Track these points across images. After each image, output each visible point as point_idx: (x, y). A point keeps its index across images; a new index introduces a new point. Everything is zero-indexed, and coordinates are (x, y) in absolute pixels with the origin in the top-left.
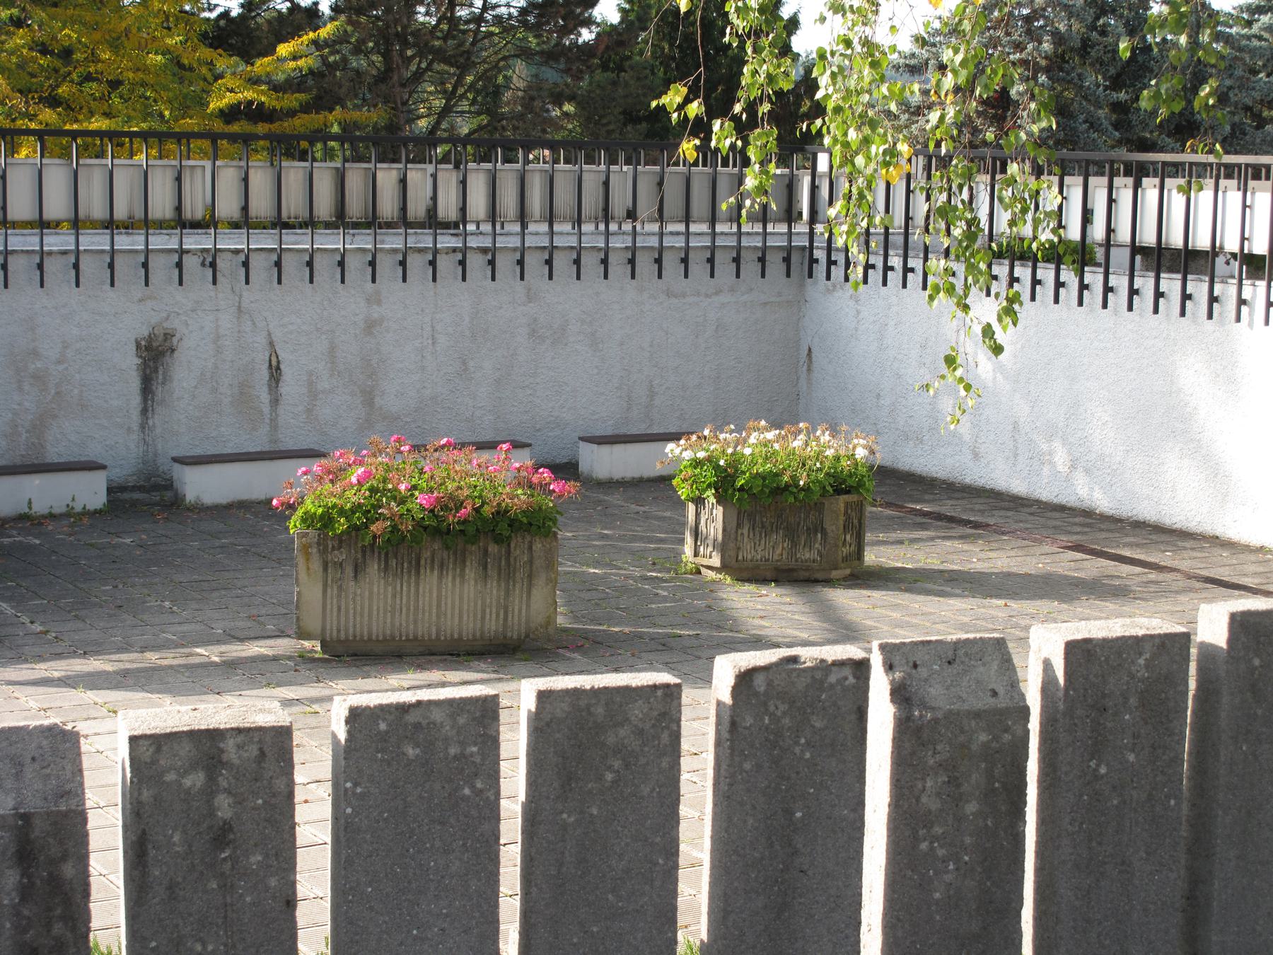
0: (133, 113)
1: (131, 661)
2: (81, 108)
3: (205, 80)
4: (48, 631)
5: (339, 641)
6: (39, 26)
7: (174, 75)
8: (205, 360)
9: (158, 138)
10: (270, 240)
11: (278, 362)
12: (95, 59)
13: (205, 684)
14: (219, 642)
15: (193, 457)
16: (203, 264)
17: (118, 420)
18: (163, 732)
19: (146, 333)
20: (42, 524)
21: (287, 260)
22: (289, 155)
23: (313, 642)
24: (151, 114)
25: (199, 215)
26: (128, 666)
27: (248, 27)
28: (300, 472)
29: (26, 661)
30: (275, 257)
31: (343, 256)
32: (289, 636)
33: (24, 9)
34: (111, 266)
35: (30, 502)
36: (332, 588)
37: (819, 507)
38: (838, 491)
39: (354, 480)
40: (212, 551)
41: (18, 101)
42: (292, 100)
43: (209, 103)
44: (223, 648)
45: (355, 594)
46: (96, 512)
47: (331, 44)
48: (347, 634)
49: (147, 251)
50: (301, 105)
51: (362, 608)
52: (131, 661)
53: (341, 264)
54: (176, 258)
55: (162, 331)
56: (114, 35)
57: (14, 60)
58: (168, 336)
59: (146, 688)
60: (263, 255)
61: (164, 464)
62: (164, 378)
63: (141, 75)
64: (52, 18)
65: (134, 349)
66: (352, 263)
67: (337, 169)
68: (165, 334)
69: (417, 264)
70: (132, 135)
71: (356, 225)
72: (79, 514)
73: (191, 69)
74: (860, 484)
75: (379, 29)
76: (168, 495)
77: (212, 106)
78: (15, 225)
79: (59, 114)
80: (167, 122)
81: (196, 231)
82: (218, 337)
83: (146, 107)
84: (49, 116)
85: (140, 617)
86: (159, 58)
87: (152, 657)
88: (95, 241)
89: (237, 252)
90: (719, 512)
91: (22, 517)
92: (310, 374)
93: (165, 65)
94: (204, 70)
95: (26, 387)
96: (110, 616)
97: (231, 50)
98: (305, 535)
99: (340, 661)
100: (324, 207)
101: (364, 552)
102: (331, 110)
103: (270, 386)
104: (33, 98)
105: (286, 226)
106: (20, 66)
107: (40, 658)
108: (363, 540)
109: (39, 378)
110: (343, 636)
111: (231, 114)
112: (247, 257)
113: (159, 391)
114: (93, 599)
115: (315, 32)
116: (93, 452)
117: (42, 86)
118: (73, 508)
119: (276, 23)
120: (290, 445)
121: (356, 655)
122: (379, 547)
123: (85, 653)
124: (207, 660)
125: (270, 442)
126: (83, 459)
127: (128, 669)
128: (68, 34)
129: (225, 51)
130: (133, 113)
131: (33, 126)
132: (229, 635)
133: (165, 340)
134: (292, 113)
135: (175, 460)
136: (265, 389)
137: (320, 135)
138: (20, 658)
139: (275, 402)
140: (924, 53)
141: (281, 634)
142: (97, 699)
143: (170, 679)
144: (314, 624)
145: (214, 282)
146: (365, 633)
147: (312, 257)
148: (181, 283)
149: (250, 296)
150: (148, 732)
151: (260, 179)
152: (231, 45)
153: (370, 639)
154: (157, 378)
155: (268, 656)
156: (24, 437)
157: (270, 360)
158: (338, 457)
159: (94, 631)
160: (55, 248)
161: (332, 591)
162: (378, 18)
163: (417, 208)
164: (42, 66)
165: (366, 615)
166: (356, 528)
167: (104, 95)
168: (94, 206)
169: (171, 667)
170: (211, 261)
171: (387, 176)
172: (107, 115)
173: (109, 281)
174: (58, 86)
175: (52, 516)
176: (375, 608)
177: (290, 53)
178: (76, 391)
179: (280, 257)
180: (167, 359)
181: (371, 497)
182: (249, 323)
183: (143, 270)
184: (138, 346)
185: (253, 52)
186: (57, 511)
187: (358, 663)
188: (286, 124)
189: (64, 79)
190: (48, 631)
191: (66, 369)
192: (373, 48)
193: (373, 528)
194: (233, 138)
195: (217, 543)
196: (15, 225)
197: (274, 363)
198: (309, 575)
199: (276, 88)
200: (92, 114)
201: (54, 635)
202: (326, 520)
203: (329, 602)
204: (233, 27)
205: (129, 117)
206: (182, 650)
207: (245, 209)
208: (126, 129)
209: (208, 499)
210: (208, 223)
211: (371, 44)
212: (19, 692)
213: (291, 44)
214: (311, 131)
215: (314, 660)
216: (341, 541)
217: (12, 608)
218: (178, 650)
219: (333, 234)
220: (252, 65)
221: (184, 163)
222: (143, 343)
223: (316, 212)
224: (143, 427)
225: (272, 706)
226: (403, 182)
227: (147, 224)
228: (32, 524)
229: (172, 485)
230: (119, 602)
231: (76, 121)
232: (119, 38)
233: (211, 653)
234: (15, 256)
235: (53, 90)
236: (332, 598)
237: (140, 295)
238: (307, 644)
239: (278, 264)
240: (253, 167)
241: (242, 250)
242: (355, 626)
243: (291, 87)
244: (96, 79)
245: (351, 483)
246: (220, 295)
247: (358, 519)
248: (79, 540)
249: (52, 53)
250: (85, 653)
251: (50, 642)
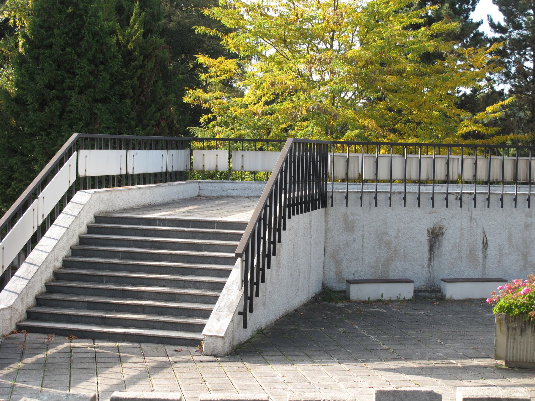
0: (426, 136)
1: (424, 364)
2: (405, 133)
3: (456, 122)
4: (390, 349)
5: (513, 361)
6: (390, 100)
7: (443, 120)
8: (456, 239)
9: (437, 146)
10: (484, 189)
11: (487, 241)
12: (411, 113)
13: (455, 375)
14: (461, 358)
15: (450, 279)
16: (456, 199)
17: (419, 262)
18: (477, 397)
19: (432, 227)
20: (387, 304)
21: (492, 198)
22: (494, 153)
23: (502, 361)
24: (433, 136)
25: (455, 178)
26: (423, 365)
27: (474, 100)
28: (498, 288)
29: (381, 360)
30: (487, 196)
31: (516, 197)
32: (491, 358)
33: (383, 94)
34: (419, 199)
35: (382, 295)
36: (511, 338)
39: (522, 292)
40: (458, 319)
41: (380, 131)
42: (492, 130)
43: (457, 131)
44: (463, 361)
45: (521, 341)
46: (409, 300)
47: (509, 106)
48: (516, 359)
49: (434, 193)
50: (496, 132)
51: (524, 348)
52: (424, 364)
53: (515, 200)
54: (445, 196)
55: (438, 226)
56: (419, 104)
57: (379, 114)
58: (441, 228)
59: (431, 375)
60: (482, 195)
61: (437, 281)
62: (439, 246)
63: (429, 120)
64: (395, 97)
65: (427, 233)
66: (520, 199)
67: (514, 160)
68: (440, 227)
70: (427, 145)
72: (402, 301)
73: (450, 117)
75: (530, 100)
76: (439, 294)
77: (458, 132)
78: (367, 181)
79: (396, 136)
80: (440, 139)
81: (453, 185)
82: (462, 229)
83: (431, 133)
84: (392, 137)
85: (427, 345)
86: (437, 113)
87: (433, 363)
88: (412, 188)
89: (471, 194)
91: (379, 301)
92: (500, 246)
93: (440, 116)
94: (456, 118)
95: (382, 247)
96: (415, 344)
97: (466, 109)
98: (500, 315)
99: (513, 370)
100: (508, 176)
101: (525, 324)
102: (508, 134)
103: (483, 251)
104: (386, 129)
105: (491, 183)
106: (381, 117)
107: (387, 360)
108: (525, 319)
109: (388, 244)
110: (515, 359)
111: (466, 136)
112: (475, 196)
113: (436, 251)
114: (408, 336)
115: (503, 101)
116: (408, 275)
117: (390, 125)
118: (399, 298)
119: (486, 98)
120: (491, 276)
121: (520, 368)
122: (532, 322)
123: (405, 359)
124: (456, 365)
125: (482, 274)
126: (404, 278)
127: (423, 367)
128: (401, 104)
129: (465, 110)
130: (426, 136)
131: (386, 141)
132: (465, 356)
133: (440, 230)
134: (492, 136)
135: (442, 280)
136: (481, 252)
137: (503, 145)
138: (378, 359)
139: (485, 257)
141: (487, 357)
142: (410, 379)
143: (441, 373)
144: (502, 353)
145: (461, 206)
146: (525, 359)
147: (502, 196)
148: (447, 206)
149: (476, 212)
150: (471, 397)
151: (482, 164)
152: (466, 107)
153: (526, 362)
154: (436, 245)
155: (481, 366)
156: (380, 268)
157: (483, 240)
158: (515, 283)
159: (408, 350)
160: (396, 191)
161: (511, 339)
162: (529, 95)
164: (390, 116)
165: (525, 351)
166: (522, 313)
167: (414, 128)
168: (413, 174)
169: (441, 367)
170: (460, 198)
172: (415, 136)
173: (417, 205)
174: (395, 125)
175: (391, 301)
176: (529, 348)
177: (492, 110)
178: (402, 250)
179: (489, 196)
180: (440, 238)
181: (529, 300)
182: (475, 224)
183: (432, 201)
184: (428, 232)
185: (476, 110)
186: (393, 299)
187: (521, 371)
188: (489, 140)
189: (398, 122)
190: (390, 349)
191: (399, 240)
192: (527, 108)
193: (530, 313)
194: (468, 146)
195: (459, 316)
196: (367, 181)
197: (485, 241)
198: (501, 332)
199: (485, 125)
200: (409, 136)
201: (392, 350)
202: (509, 309)
203: (509, 344)
204: (468, 100)
205: (425, 137)
206: (445, 361)
207: (475, 176)
208: (423, 142)
209: (455, 297)
210: (460, 181)
211: (526, 107)
212: (379, 373)
213: (493, 107)
214: (500, 143)
215: (501, 369)
216: (515, 319)
217: (375, 338)
218: (444, 361)
219: (511, 187)
220: (476, 115)
221: (393, 155)
222: (430, 231)
223: (505, 178)
224: (429, 265)
225: (521, 390)
227: (434, 182)
228: (383, 304)
229: (440, 290)
230: (419, 339)
231: (403, 139)
232: (421, 105)
233: (458, 363)
234: (380, 193)
235: (394, 126)
236: (510, 343)
237: (430, 211)
238: (499, 362)
239: (488, 199)
240: (533, 160)
241: (473, 193)
242: (520, 355)
243: (491, 124)
244: (412, 122)
245: (520, 294)
246: (463, 212)
247: (524, 310)
248: (402, 312)
249: (394, 111)
250: (405, 359)
251: (391, 353)
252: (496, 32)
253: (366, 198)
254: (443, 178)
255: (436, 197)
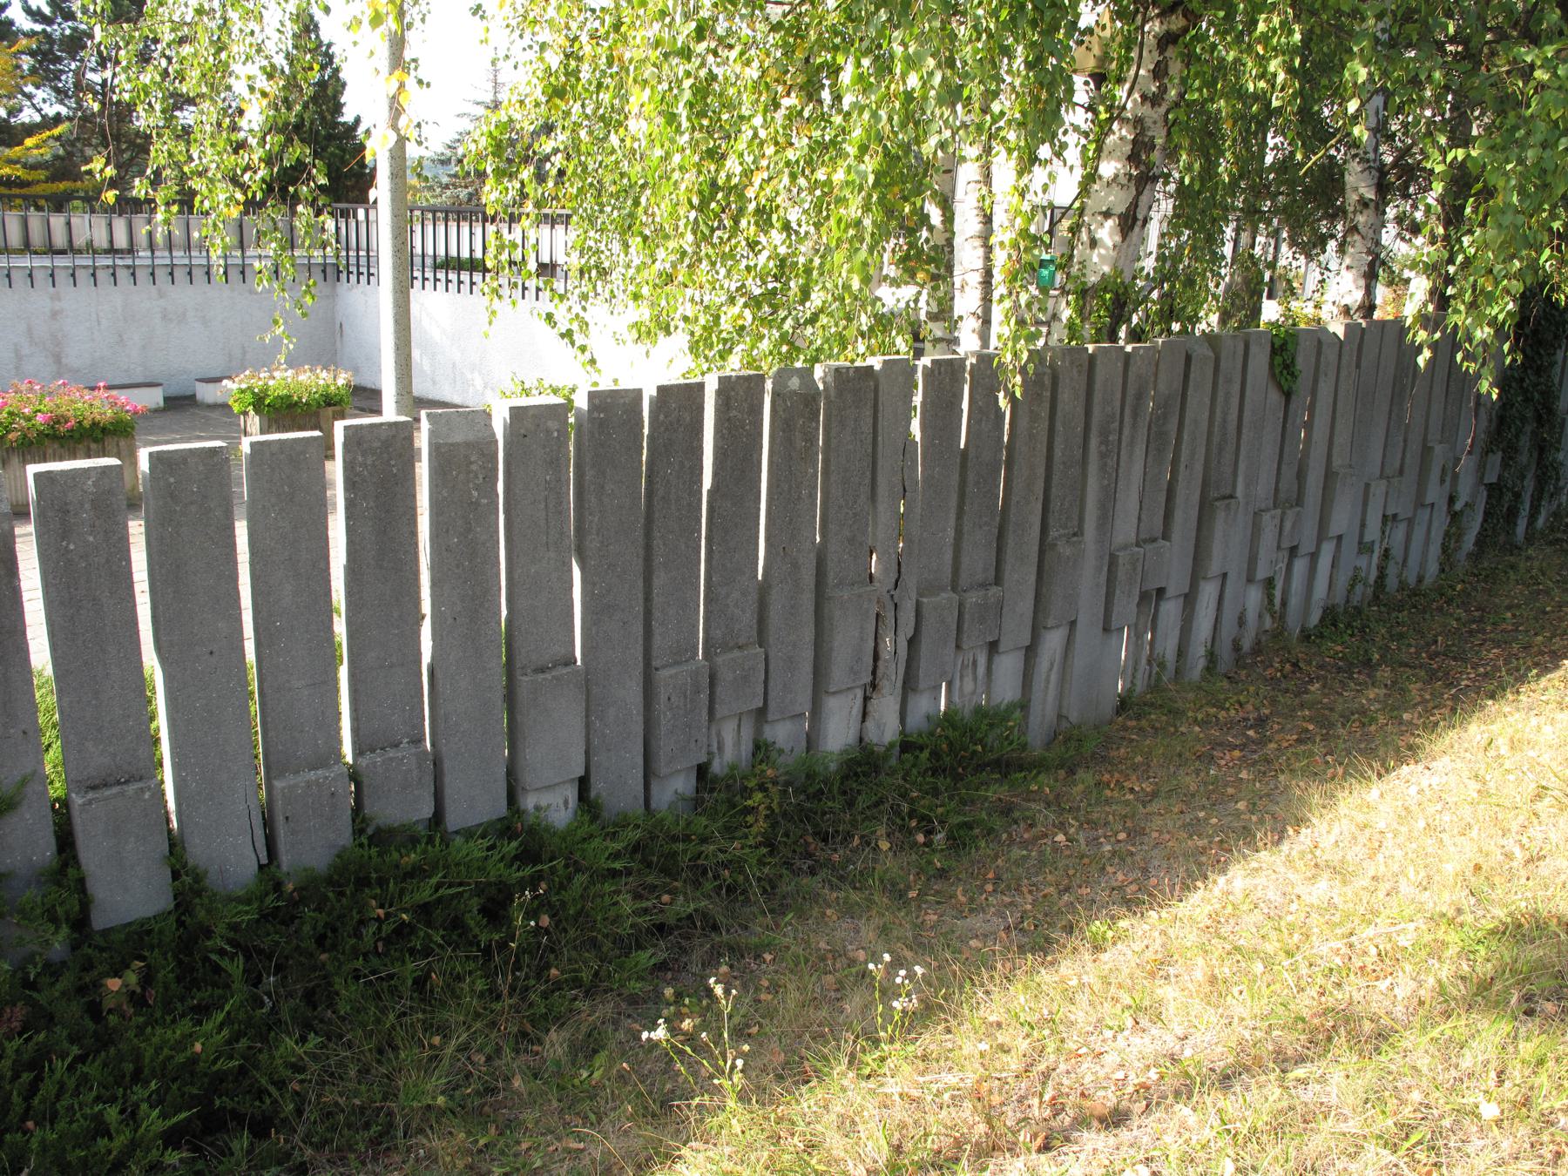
37: (317, 414)
38: (329, 404)
42: (42, 174)
69: (123, 275)
71: (36, 253)
74: (341, 400)
89: (67, 268)
90: (257, 419)
140: (448, 153)
163: (80, 241)
171: (57, 221)
199: (25, 166)
226: (69, 224)
252: (36, 21)
253: (100, 274)
254: (105, 245)
255: (99, 274)
